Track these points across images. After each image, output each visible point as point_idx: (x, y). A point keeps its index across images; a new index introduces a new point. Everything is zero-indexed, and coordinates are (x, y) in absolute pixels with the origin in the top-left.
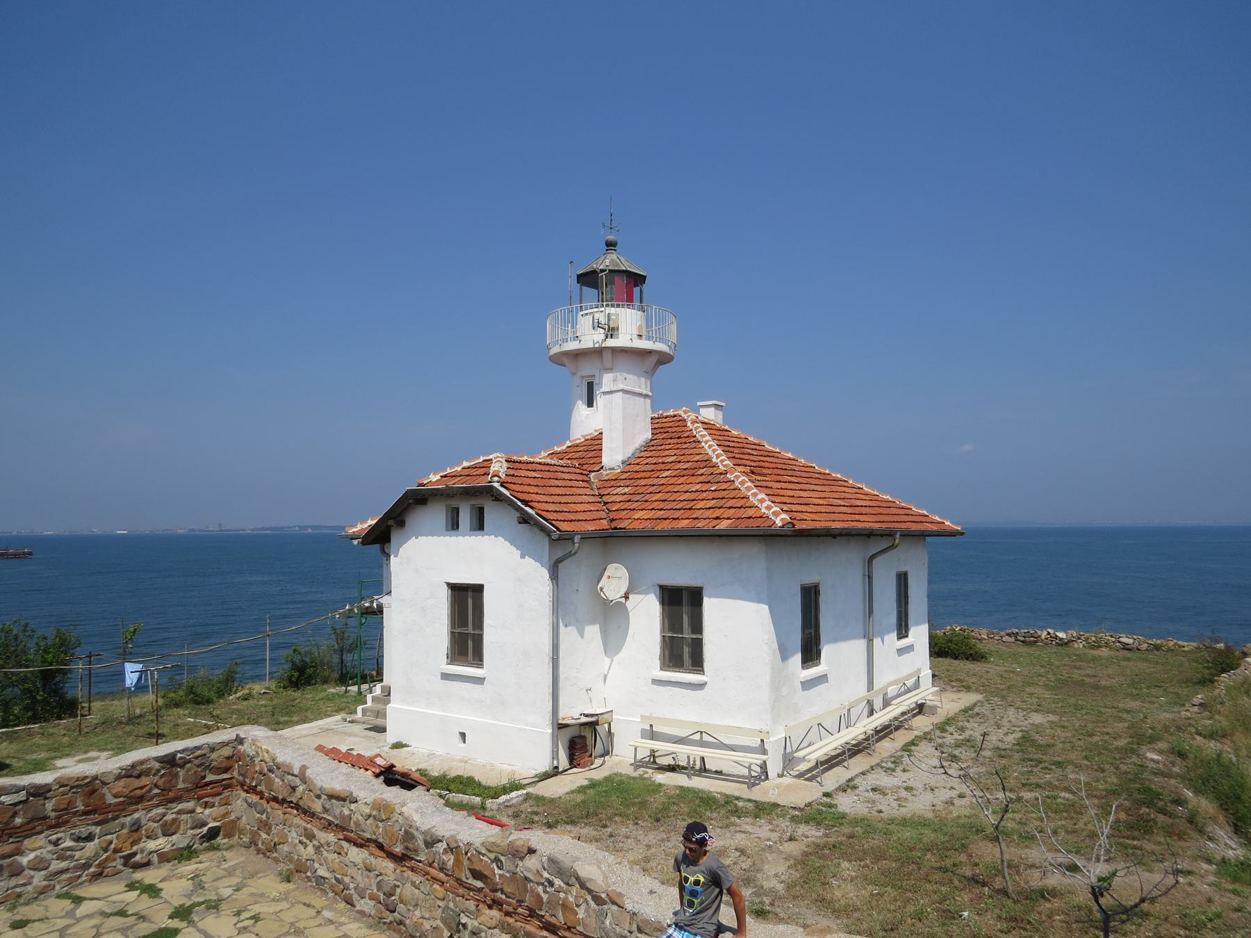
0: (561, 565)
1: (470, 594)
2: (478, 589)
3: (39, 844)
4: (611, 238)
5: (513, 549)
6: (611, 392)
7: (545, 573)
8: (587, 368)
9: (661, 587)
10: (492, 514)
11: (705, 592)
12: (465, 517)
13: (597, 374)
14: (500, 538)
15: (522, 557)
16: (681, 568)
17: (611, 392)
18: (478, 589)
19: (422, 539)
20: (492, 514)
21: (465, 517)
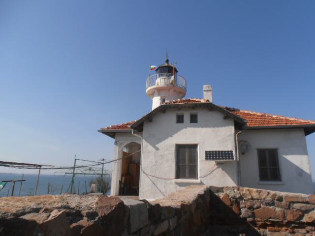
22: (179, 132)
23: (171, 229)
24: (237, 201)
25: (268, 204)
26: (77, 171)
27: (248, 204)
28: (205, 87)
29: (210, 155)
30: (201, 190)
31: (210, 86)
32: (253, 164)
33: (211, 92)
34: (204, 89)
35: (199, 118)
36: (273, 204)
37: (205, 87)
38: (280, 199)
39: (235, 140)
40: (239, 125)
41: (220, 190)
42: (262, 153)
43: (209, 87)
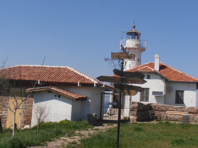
22: (153, 80)
23: (190, 123)
24: (155, 106)
25: (162, 107)
26: (105, 108)
27: (158, 107)
28: (156, 56)
29: (154, 93)
30: (38, 103)
31: (159, 55)
32: (173, 96)
33: (159, 59)
34: (155, 57)
35: (151, 77)
36: (163, 107)
37: (156, 56)
38: (164, 106)
39: (165, 87)
40: (166, 81)
41: (152, 104)
42: (177, 92)
43: (158, 56)
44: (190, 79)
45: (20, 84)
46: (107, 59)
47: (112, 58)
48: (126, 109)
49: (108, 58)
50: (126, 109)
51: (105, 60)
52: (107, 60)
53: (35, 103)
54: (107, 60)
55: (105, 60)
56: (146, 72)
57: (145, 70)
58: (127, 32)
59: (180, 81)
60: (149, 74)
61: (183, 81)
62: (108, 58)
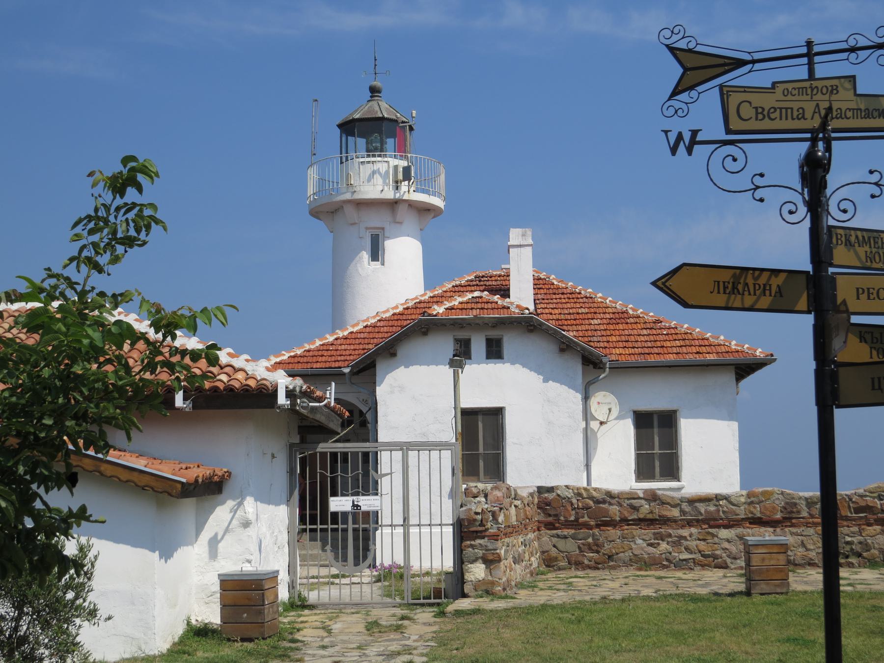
0: (592, 387)
1: (480, 417)
2: (497, 413)
3: (732, 584)
4: (377, 84)
5: (533, 375)
6: (520, 246)
7: (579, 396)
8: (375, 220)
9: (635, 412)
10: (511, 342)
11: (79, 477)
12: (478, 346)
13: (387, 226)
14: (517, 366)
15: (546, 380)
16: (656, 396)
17: (520, 246)
18: (497, 413)
19: (415, 369)
20: (511, 342)
21: (478, 346)
36: (604, 502)
37: (515, 236)
44: (704, 349)
45: (5, 371)
46: (687, 137)
47: (728, 131)
48: (387, 531)
49: (695, 133)
50: (387, 531)
51: (674, 150)
52: (690, 151)
53: (273, 576)
54: (690, 151)
55: (674, 150)
56: (480, 322)
57: (475, 312)
58: (338, 122)
59: (652, 359)
60: (494, 334)
61: (672, 358)
62: (695, 133)
